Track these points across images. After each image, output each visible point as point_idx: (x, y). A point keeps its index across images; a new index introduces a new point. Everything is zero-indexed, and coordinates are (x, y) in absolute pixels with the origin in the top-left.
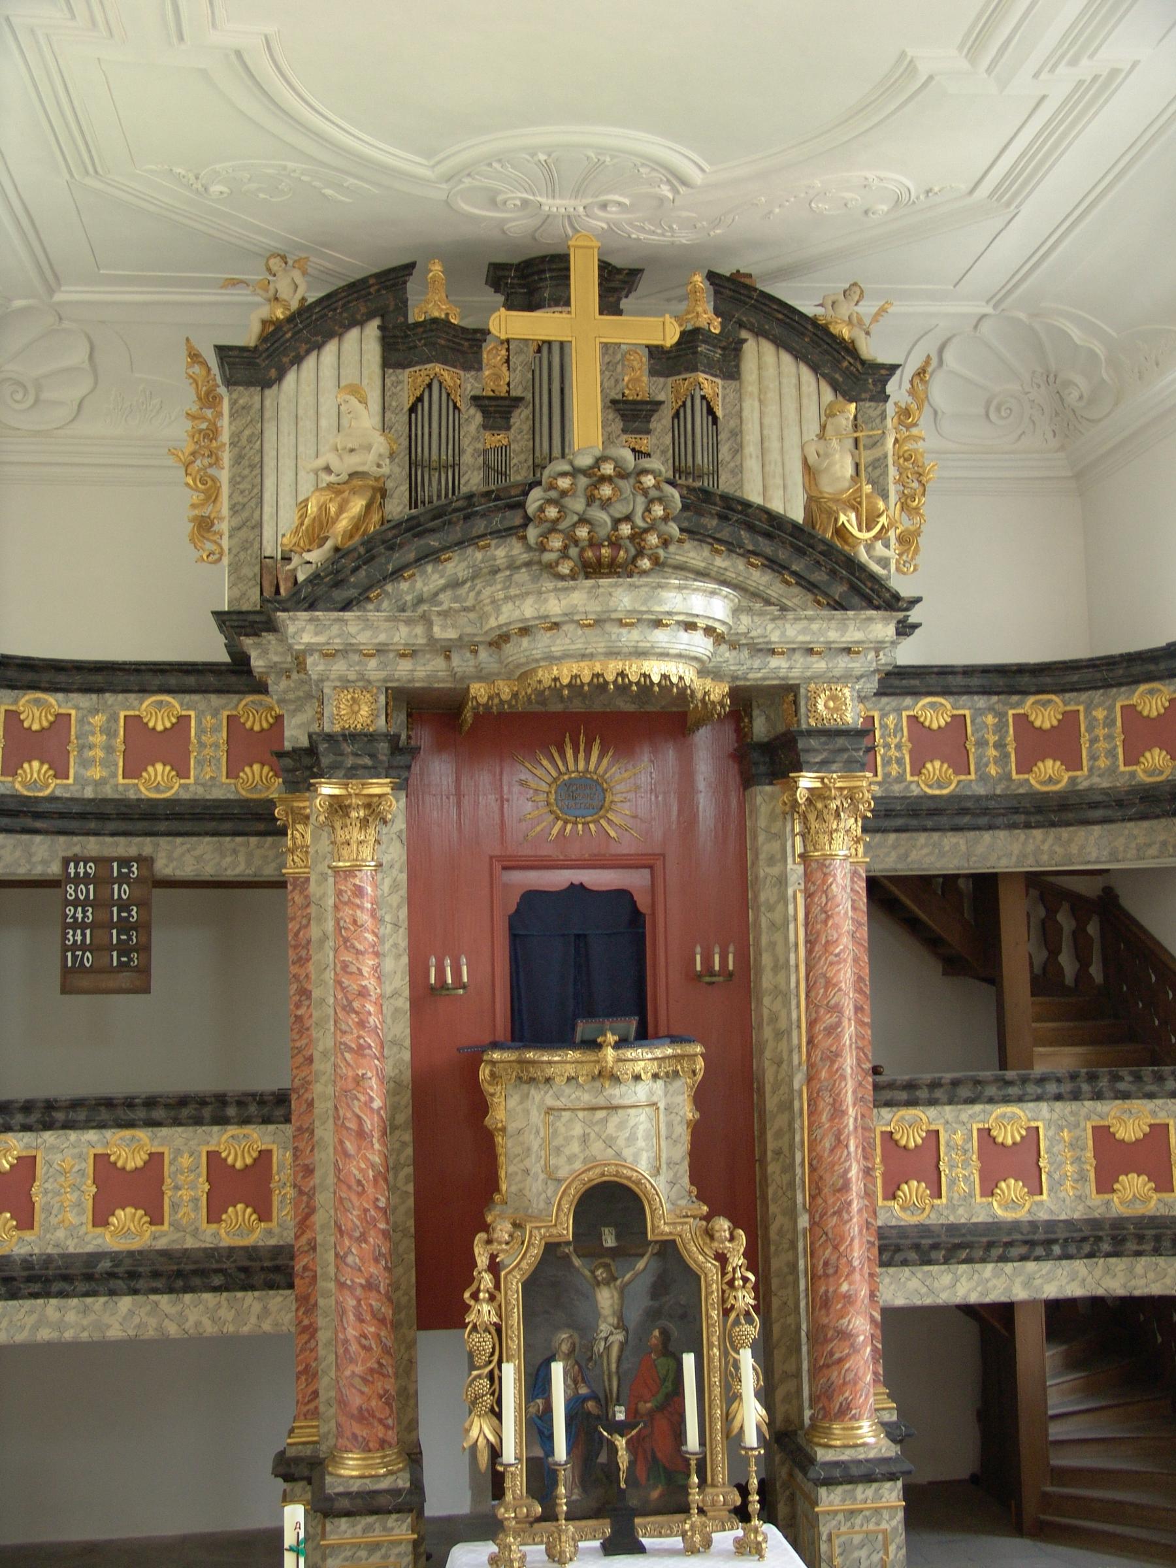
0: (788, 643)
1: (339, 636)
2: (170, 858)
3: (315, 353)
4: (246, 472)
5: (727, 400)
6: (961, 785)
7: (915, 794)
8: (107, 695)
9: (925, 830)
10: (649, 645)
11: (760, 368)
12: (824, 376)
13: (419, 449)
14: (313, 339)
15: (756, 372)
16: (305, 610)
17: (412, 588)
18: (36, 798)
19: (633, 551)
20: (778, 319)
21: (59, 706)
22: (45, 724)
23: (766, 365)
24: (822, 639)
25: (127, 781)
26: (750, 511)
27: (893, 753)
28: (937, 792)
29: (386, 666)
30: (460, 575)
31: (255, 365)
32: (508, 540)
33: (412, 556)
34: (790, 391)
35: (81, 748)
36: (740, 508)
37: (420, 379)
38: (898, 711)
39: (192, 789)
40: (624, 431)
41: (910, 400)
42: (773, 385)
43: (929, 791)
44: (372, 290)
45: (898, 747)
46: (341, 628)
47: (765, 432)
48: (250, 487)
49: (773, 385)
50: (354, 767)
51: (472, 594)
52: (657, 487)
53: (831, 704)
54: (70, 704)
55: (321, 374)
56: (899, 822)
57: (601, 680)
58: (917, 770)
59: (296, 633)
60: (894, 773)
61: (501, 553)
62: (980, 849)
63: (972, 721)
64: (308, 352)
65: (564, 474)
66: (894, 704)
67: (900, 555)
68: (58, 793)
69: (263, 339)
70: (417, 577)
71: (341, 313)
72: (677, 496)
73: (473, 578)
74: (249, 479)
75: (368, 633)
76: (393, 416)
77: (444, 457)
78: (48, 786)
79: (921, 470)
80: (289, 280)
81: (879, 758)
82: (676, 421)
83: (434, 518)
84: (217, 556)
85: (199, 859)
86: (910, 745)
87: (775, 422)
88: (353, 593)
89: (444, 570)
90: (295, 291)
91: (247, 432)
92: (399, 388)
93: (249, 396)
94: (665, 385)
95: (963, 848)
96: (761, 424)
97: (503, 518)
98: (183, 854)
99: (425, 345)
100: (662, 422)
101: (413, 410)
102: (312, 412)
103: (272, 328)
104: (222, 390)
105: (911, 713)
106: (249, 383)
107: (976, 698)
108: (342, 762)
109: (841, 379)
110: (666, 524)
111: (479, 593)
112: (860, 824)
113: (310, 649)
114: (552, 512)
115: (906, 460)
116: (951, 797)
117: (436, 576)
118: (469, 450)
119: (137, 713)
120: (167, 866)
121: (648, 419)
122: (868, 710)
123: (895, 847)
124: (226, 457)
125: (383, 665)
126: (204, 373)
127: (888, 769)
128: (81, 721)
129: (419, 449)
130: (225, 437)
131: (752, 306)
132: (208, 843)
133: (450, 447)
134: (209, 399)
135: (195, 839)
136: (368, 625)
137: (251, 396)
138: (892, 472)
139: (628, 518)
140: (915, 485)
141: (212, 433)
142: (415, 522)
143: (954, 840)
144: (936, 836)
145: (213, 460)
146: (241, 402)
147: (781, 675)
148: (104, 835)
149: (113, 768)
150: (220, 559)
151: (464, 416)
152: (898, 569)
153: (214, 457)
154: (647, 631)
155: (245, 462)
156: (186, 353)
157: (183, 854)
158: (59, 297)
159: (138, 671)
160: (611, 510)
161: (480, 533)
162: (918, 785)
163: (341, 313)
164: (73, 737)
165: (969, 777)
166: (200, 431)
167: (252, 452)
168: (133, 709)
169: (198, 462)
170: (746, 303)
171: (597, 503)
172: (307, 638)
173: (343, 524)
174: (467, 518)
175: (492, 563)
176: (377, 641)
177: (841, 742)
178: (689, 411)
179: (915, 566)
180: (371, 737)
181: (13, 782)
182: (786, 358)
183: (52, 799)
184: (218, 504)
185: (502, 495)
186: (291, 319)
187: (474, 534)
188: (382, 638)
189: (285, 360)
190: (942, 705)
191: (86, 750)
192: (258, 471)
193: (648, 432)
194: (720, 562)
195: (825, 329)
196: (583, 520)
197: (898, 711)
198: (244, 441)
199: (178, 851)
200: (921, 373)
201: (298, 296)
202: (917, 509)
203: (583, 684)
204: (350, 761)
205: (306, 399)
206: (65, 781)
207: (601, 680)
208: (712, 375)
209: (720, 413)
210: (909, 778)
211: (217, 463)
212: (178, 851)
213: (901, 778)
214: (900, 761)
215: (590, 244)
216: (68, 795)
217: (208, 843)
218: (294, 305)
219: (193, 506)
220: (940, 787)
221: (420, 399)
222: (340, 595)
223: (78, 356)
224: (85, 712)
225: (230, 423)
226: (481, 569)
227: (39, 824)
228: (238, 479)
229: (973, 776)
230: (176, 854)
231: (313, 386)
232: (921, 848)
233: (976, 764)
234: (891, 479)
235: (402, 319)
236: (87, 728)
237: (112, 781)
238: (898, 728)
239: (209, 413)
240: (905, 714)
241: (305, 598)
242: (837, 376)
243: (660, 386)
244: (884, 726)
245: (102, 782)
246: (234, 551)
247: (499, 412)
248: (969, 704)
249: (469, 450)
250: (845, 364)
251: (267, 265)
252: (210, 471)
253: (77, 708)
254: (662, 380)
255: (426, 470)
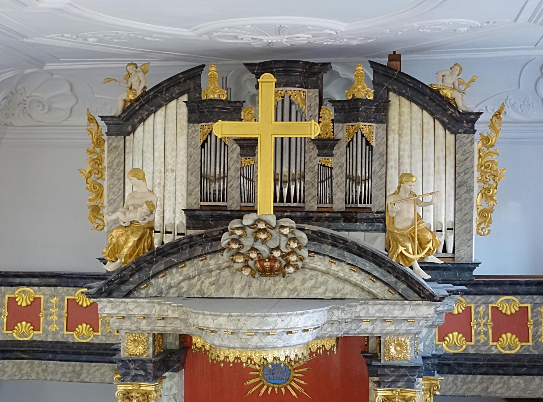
0: (370, 317)
1: (124, 310)
2: (88, 373)
3: (153, 115)
4: (116, 182)
5: (379, 135)
6: (523, 348)
7: (494, 352)
8: (59, 288)
9: (499, 374)
10: (264, 344)
11: (400, 115)
12: (438, 119)
13: (206, 169)
14: (151, 109)
15: (397, 117)
16: (106, 297)
17: (165, 281)
18: (23, 341)
19: (284, 263)
20: (410, 86)
21: (36, 294)
22: (29, 303)
23: (403, 111)
24: (390, 316)
25: (68, 333)
26: (347, 243)
27: (482, 328)
28: (508, 352)
29: (151, 324)
30: (191, 274)
31: (126, 121)
32: (217, 255)
33: (162, 267)
34: (417, 128)
35: (46, 315)
36: (342, 242)
37: (205, 130)
38: (486, 303)
39: (100, 337)
40: (319, 155)
41: (490, 131)
42: (407, 125)
43: (504, 352)
44: (181, 80)
45: (485, 325)
46: (125, 306)
47: (401, 153)
48: (118, 190)
49: (407, 125)
50: (136, 375)
51: (199, 283)
52: (292, 232)
53: (398, 348)
54: (40, 293)
55: (155, 127)
56: (483, 370)
57: (239, 361)
58: (496, 339)
59: (102, 308)
60: (482, 340)
61: (212, 262)
62: (533, 386)
63: (532, 311)
64: (148, 116)
65: (238, 228)
66: (484, 300)
67: (479, 224)
68: (35, 339)
69: (124, 111)
70: (168, 276)
71: (165, 94)
72: (305, 236)
73: (199, 275)
74: (118, 186)
75: (139, 309)
76: (192, 150)
77: (218, 173)
78: (30, 335)
79: (495, 173)
80: (137, 78)
81: (473, 331)
82: (348, 149)
83: (172, 248)
84: (102, 227)
85: (102, 374)
86: (492, 324)
87: (408, 147)
88: (131, 287)
89: (182, 272)
90: (140, 84)
91: (117, 161)
92: (196, 134)
93: (118, 141)
94: (342, 128)
95: (522, 385)
96: (399, 148)
97: (212, 246)
98: (95, 372)
99: (208, 111)
100: (340, 150)
101: (203, 146)
102: (150, 148)
103: (129, 104)
104: (105, 137)
105: (494, 305)
106: (117, 134)
107: (535, 297)
108: (130, 372)
109: (447, 121)
110: (300, 250)
111: (203, 282)
112: (432, 398)
113: (111, 316)
114: (235, 246)
115: (485, 168)
116: (516, 355)
117: (178, 275)
118: (233, 168)
119: (73, 297)
120: (87, 377)
121: (332, 148)
122: (468, 303)
123: (480, 383)
124: (106, 174)
125: (149, 324)
126: (96, 128)
127: (479, 338)
128: (46, 301)
129: (206, 169)
130: (105, 164)
131: (395, 79)
132: (107, 366)
133: (222, 167)
134: (99, 143)
135: (101, 364)
136: (139, 305)
137: (118, 141)
138: (476, 175)
139: (278, 248)
140: (492, 182)
141: (98, 161)
142: (161, 251)
143: (517, 381)
144: (506, 377)
145: (99, 176)
146: (113, 144)
147: (368, 332)
148: (57, 360)
149: (62, 325)
150: (103, 229)
151: (230, 149)
152: (478, 233)
153: (100, 172)
154: (262, 337)
155: (115, 177)
156: (87, 117)
157: (95, 372)
158: (45, 68)
159: (72, 278)
160: (268, 244)
161: (199, 254)
162: (496, 347)
163: (165, 94)
164: (42, 309)
165: (528, 344)
166: (94, 160)
167: (119, 171)
168: (72, 296)
169: (93, 177)
170: (392, 78)
171: (260, 240)
172: (107, 311)
173: (126, 251)
174: (191, 247)
175: (208, 267)
176: (143, 313)
177: (403, 371)
178: (355, 144)
179: (489, 231)
180: (144, 362)
181: (12, 334)
182: (415, 107)
183: (32, 342)
184: (102, 200)
185: (208, 235)
186: (137, 100)
187: (196, 254)
188: (146, 311)
189: (136, 121)
190: (513, 300)
191: (49, 316)
192: (122, 181)
193: (332, 156)
194: (335, 268)
195: (437, 92)
196: (253, 249)
197: (486, 303)
198: (115, 166)
199: (93, 370)
200: (497, 115)
201: (142, 87)
202: (491, 197)
203: (230, 362)
204: (133, 373)
205: (149, 141)
206: (38, 332)
207: (239, 361)
208: (369, 122)
209: (373, 144)
210: (491, 343)
211: (102, 177)
212: (93, 370)
213: (486, 343)
214: (486, 333)
215: (270, 80)
216: (39, 339)
217: (107, 366)
218: (139, 93)
219: (90, 200)
220: (510, 349)
221: (206, 141)
222: (125, 288)
223: (66, 89)
224: (48, 297)
225: (108, 156)
226: (202, 271)
227: (24, 356)
228: (112, 186)
229: (530, 343)
230: (91, 372)
231: (152, 134)
232: (496, 385)
233: (533, 336)
234: (476, 179)
235: (198, 95)
236: (49, 304)
237: (61, 332)
238: (486, 314)
239: (98, 150)
240: (490, 306)
241: (104, 292)
242: (445, 119)
243: (340, 128)
244: (477, 313)
245: (56, 333)
246: (110, 225)
247: (249, 146)
248: (530, 300)
249: (233, 168)
250: (450, 112)
251: (126, 69)
252: (98, 181)
253: (44, 294)
254: (341, 125)
255: (208, 180)
